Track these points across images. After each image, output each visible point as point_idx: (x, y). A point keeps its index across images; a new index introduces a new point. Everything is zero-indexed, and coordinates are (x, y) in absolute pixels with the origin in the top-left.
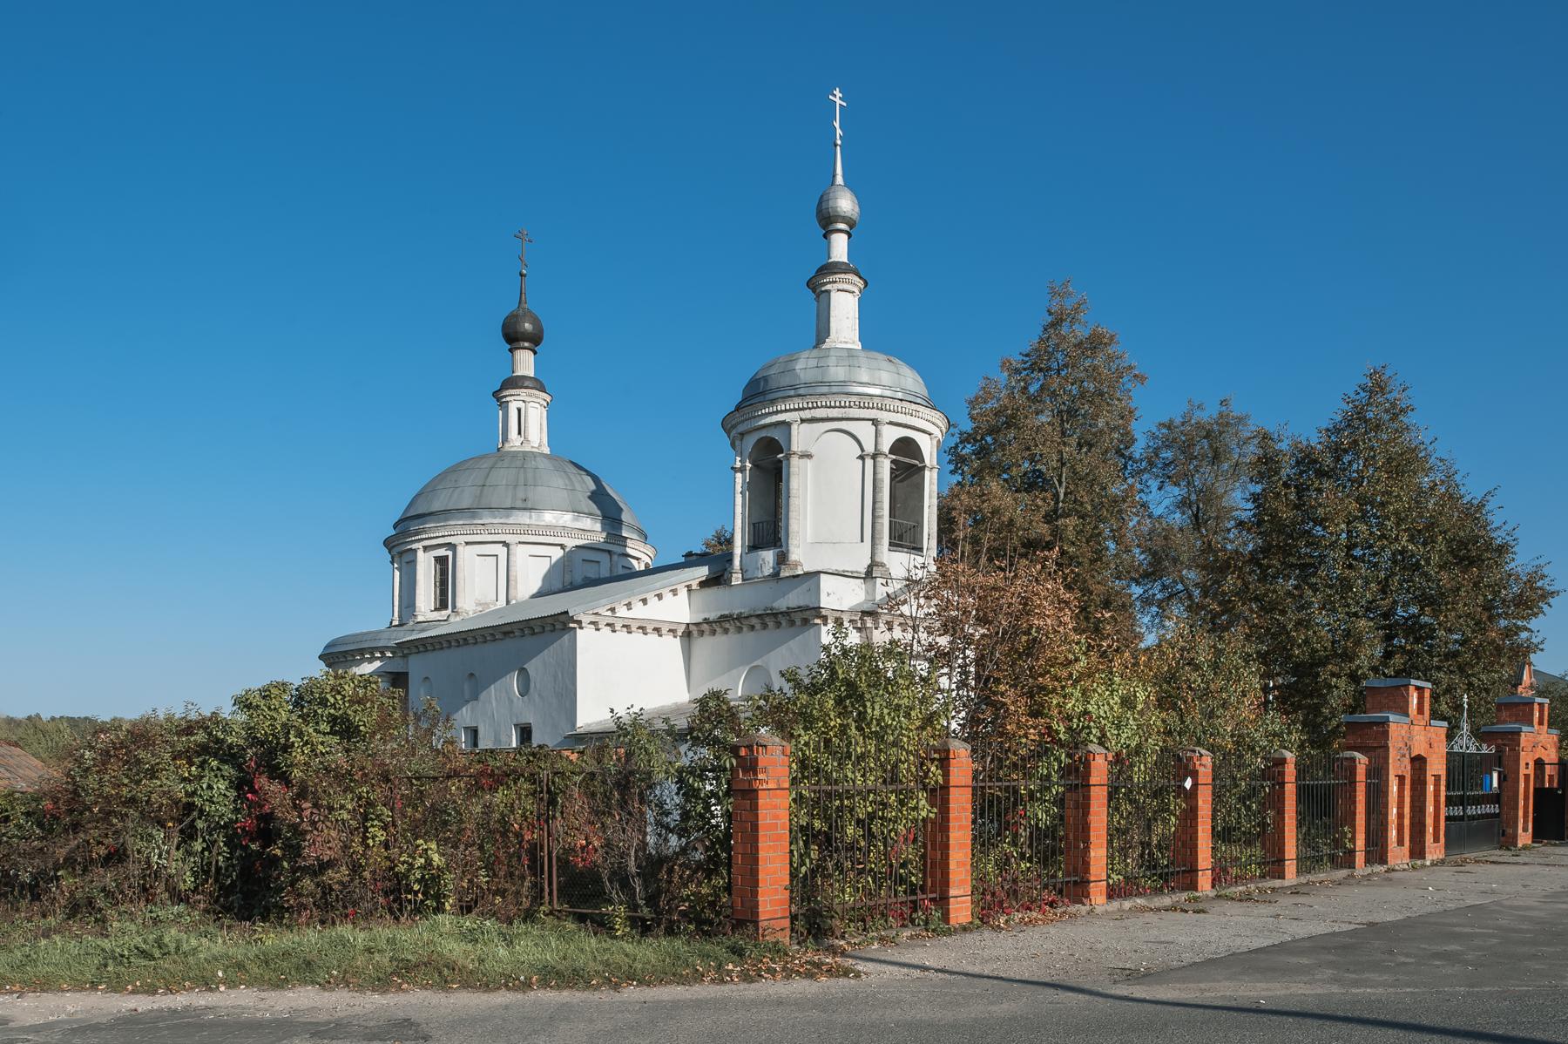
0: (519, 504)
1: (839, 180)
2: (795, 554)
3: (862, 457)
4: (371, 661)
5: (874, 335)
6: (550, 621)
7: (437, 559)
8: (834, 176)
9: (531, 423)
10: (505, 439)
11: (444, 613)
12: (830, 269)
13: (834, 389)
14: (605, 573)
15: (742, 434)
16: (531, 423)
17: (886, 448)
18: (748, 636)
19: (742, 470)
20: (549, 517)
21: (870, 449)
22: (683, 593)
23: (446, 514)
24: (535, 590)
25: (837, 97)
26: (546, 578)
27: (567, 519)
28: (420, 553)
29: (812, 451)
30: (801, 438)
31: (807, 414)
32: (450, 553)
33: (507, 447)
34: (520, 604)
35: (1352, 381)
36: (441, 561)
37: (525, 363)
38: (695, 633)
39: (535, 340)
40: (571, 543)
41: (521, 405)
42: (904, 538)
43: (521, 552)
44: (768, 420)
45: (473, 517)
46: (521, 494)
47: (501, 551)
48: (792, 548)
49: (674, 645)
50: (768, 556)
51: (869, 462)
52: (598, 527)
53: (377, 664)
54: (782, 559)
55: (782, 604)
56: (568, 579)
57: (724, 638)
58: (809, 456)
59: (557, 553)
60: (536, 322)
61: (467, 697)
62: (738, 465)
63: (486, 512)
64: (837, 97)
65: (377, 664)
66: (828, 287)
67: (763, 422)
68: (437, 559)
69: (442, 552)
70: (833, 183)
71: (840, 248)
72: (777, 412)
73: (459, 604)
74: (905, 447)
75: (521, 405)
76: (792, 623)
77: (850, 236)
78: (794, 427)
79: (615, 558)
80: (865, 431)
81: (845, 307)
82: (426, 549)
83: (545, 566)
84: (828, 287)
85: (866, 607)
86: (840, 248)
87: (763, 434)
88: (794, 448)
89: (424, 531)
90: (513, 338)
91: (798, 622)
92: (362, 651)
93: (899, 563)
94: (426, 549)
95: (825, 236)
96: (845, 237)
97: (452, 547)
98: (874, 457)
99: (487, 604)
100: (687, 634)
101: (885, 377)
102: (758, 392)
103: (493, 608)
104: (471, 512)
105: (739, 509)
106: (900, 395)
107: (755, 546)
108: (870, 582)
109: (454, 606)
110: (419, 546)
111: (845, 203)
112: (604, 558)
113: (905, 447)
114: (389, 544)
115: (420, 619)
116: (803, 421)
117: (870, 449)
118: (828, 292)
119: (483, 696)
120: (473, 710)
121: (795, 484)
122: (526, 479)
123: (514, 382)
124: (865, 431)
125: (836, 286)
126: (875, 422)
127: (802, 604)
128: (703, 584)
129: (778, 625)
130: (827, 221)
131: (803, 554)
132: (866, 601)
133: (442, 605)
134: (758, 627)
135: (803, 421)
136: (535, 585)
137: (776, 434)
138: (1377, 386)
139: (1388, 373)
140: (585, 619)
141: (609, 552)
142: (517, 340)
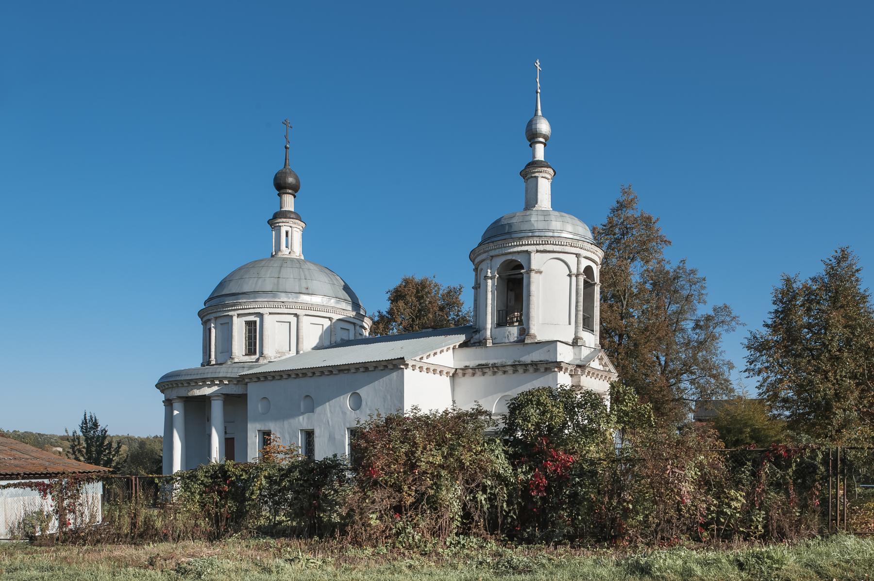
0: (304, 291)
1: (540, 113)
2: (534, 330)
3: (570, 275)
4: (209, 386)
5: (556, 204)
6: (385, 364)
7: (248, 323)
8: (536, 110)
9: (293, 238)
10: (278, 249)
11: (253, 358)
12: (534, 164)
13: (537, 234)
14: (352, 337)
15: (492, 257)
16: (293, 238)
17: (582, 270)
18: (500, 376)
19: (492, 278)
20: (316, 300)
21: (574, 271)
22: (451, 351)
23: (255, 293)
24: (314, 345)
25: (538, 64)
26: (321, 338)
27: (332, 302)
28: (235, 318)
29: (542, 269)
30: (537, 261)
31: (541, 248)
32: (258, 320)
33: (280, 255)
34: (306, 354)
35: (829, 253)
36: (251, 325)
37: (289, 203)
38: (460, 375)
39: (295, 189)
40: (336, 317)
41: (289, 229)
42: (588, 325)
43: (305, 321)
44: (516, 249)
45: (274, 297)
46: (304, 285)
47: (293, 320)
48: (531, 326)
49: (446, 381)
50: (513, 331)
51: (574, 278)
52: (350, 308)
53: (215, 388)
54: (524, 332)
55: (527, 359)
56: (333, 340)
57: (482, 378)
58: (541, 272)
59: (327, 323)
60: (297, 178)
61: (302, 410)
62: (489, 274)
63: (283, 294)
64: (538, 64)
65: (215, 388)
66: (537, 174)
67: (512, 250)
68: (248, 323)
69: (251, 318)
70: (536, 114)
71: (540, 152)
72: (522, 245)
73: (266, 352)
74: (588, 271)
75: (289, 229)
76: (536, 370)
77: (545, 145)
78: (532, 255)
79: (358, 327)
80: (572, 260)
81: (544, 187)
82: (239, 315)
83: (320, 332)
84: (537, 174)
85: (578, 362)
86: (540, 152)
87: (510, 257)
88: (533, 267)
89: (240, 304)
90: (281, 186)
91: (542, 370)
92: (204, 380)
93: (586, 336)
94: (239, 315)
95: (531, 146)
96: (542, 146)
97: (261, 315)
98: (577, 276)
99: (283, 353)
100: (454, 376)
101: (569, 228)
102: (499, 233)
103: (288, 356)
104: (273, 293)
105: (489, 301)
106: (578, 238)
107: (502, 322)
108: (577, 349)
109: (261, 353)
110: (235, 313)
111: (544, 127)
112: (351, 327)
113: (588, 271)
114: (201, 314)
115: (236, 360)
116: (537, 251)
117: (574, 271)
118: (536, 177)
119: (318, 410)
120: (308, 419)
121: (533, 288)
122: (305, 276)
123: (284, 214)
124: (572, 260)
125: (541, 175)
126: (578, 256)
127: (542, 359)
128: (461, 346)
129: (525, 371)
130: (532, 136)
131: (539, 331)
132: (575, 359)
133: (251, 351)
134: (511, 372)
135: (537, 251)
136: (315, 342)
137: (520, 259)
138: (843, 257)
139: (849, 250)
140: (411, 363)
141: (354, 324)
142: (286, 188)
